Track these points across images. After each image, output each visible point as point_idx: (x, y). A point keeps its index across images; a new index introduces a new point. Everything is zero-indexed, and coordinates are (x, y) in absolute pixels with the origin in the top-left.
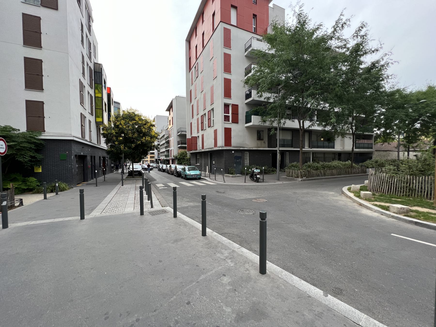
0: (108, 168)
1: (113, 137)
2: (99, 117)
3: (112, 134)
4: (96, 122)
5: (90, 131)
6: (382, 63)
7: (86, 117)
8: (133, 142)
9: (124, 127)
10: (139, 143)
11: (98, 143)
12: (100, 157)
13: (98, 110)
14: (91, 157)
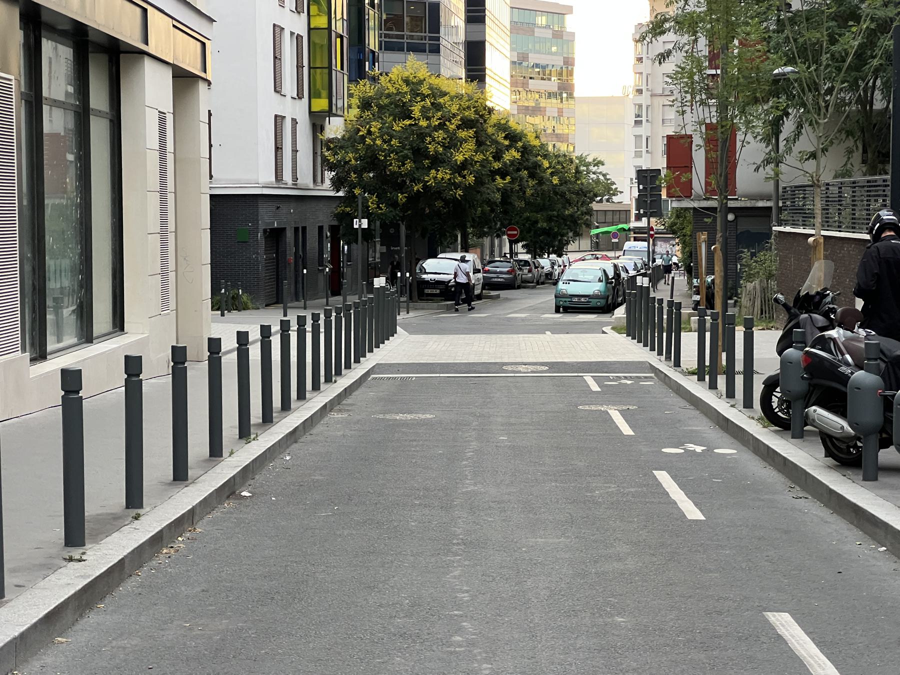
0: (350, 269)
1: (348, 173)
2: (319, 96)
3: (346, 163)
4: (310, 112)
5: (295, 151)
6: (584, 155)
7: (284, 29)
8: (401, 187)
9: (378, 142)
10: (418, 191)
11: (315, 181)
12: (321, 229)
13: (318, 71)
14: (296, 229)
